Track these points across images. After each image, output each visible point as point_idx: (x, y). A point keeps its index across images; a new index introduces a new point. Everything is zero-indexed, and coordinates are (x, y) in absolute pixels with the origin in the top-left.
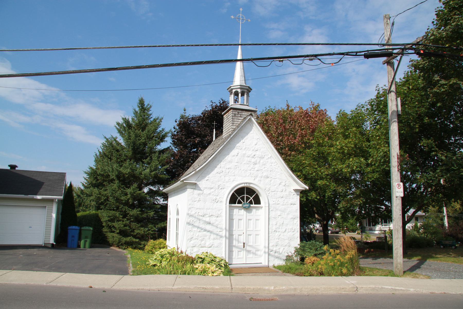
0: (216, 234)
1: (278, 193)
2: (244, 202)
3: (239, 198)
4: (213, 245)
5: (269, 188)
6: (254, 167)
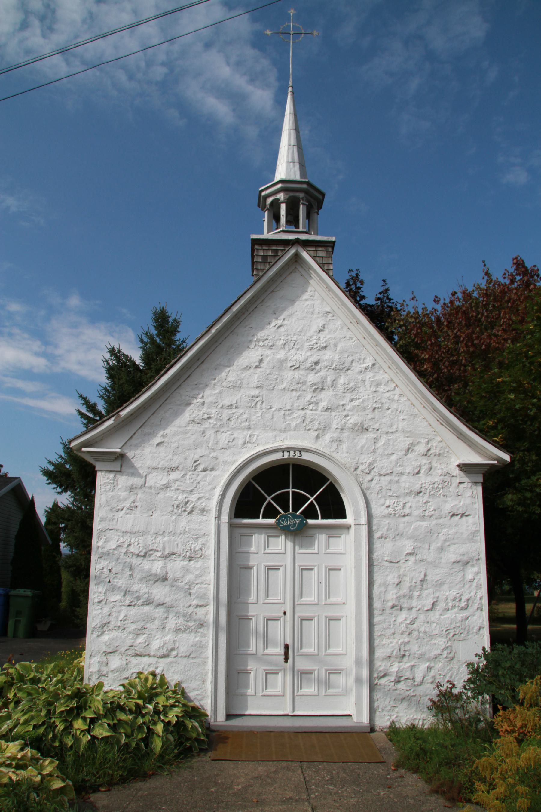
0: (184, 616)
1: (404, 478)
2: (286, 509)
3: (269, 499)
4: (173, 649)
5: (370, 464)
6: (314, 400)
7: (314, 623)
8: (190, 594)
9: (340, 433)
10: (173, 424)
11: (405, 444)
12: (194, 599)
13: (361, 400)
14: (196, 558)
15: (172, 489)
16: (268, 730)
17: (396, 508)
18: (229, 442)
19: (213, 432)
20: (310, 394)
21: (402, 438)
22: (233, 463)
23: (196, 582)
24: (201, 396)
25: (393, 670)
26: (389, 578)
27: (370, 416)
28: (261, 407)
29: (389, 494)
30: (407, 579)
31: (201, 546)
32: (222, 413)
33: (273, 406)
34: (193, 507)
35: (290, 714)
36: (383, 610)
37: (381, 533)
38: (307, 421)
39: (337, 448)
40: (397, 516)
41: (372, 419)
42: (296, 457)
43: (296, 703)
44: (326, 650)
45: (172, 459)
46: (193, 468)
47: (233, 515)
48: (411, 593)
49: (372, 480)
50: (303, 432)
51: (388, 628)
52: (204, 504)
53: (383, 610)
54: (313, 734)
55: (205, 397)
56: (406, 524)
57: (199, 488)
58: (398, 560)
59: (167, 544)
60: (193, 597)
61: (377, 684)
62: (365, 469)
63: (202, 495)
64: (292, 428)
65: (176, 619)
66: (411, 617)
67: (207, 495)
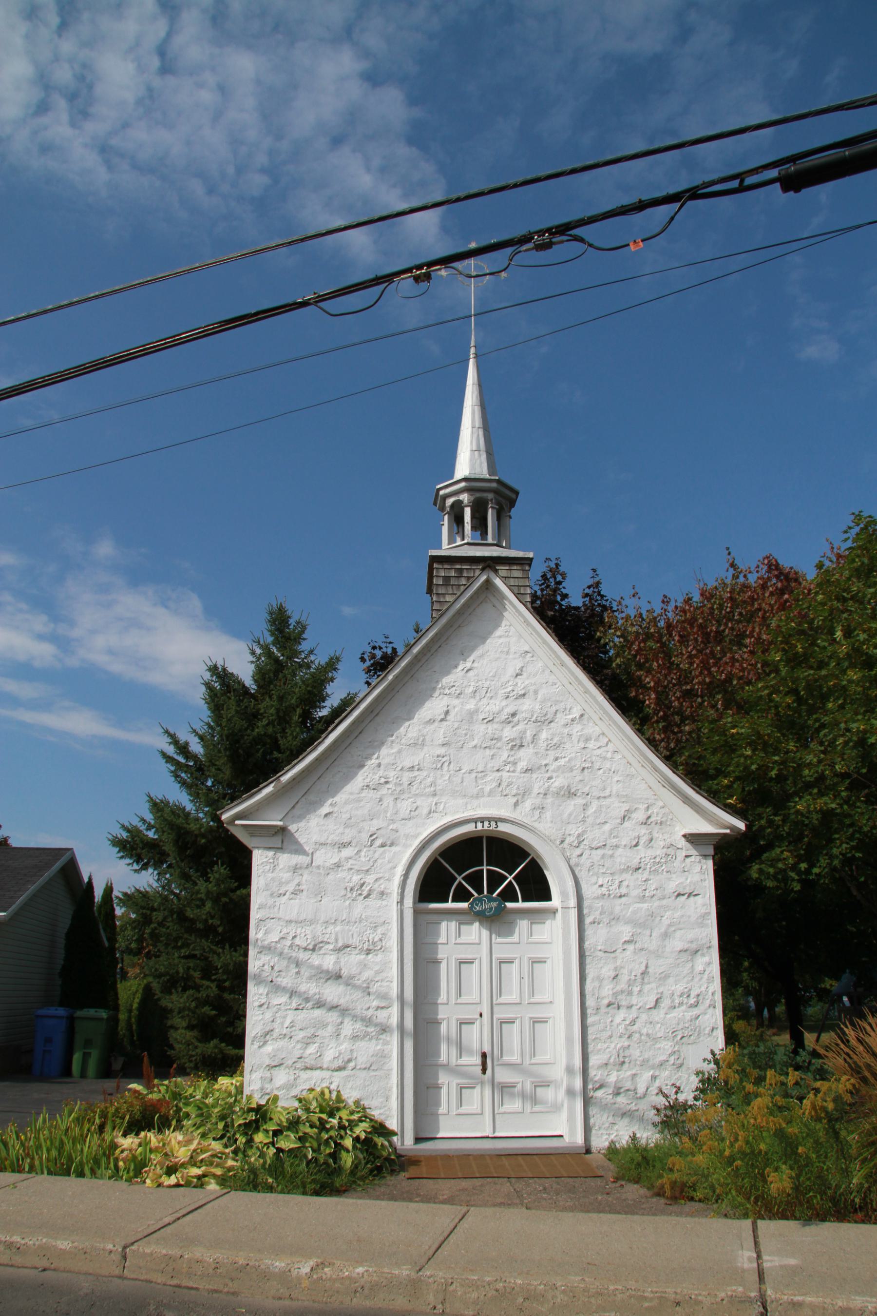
0: (363, 1019)
2: (480, 891)
3: (459, 879)
4: (349, 1061)
5: (579, 836)
6: (511, 759)
7: (516, 1027)
8: (369, 994)
10: (344, 789)
17: (611, 888)
21: (617, 804)
22: (416, 836)
24: (376, 756)
26: (604, 971)
27: (578, 778)
30: (625, 971)
34: (370, 890)
38: (504, 784)
41: (581, 781)
49: (581, 855)
51: (603, 1030)
52: (382, 887)
59: (340, 936)
60: (372, 997)
61: (592, 1097)
63: (381, 875)
64: (486, 794)
67: (387, 875)
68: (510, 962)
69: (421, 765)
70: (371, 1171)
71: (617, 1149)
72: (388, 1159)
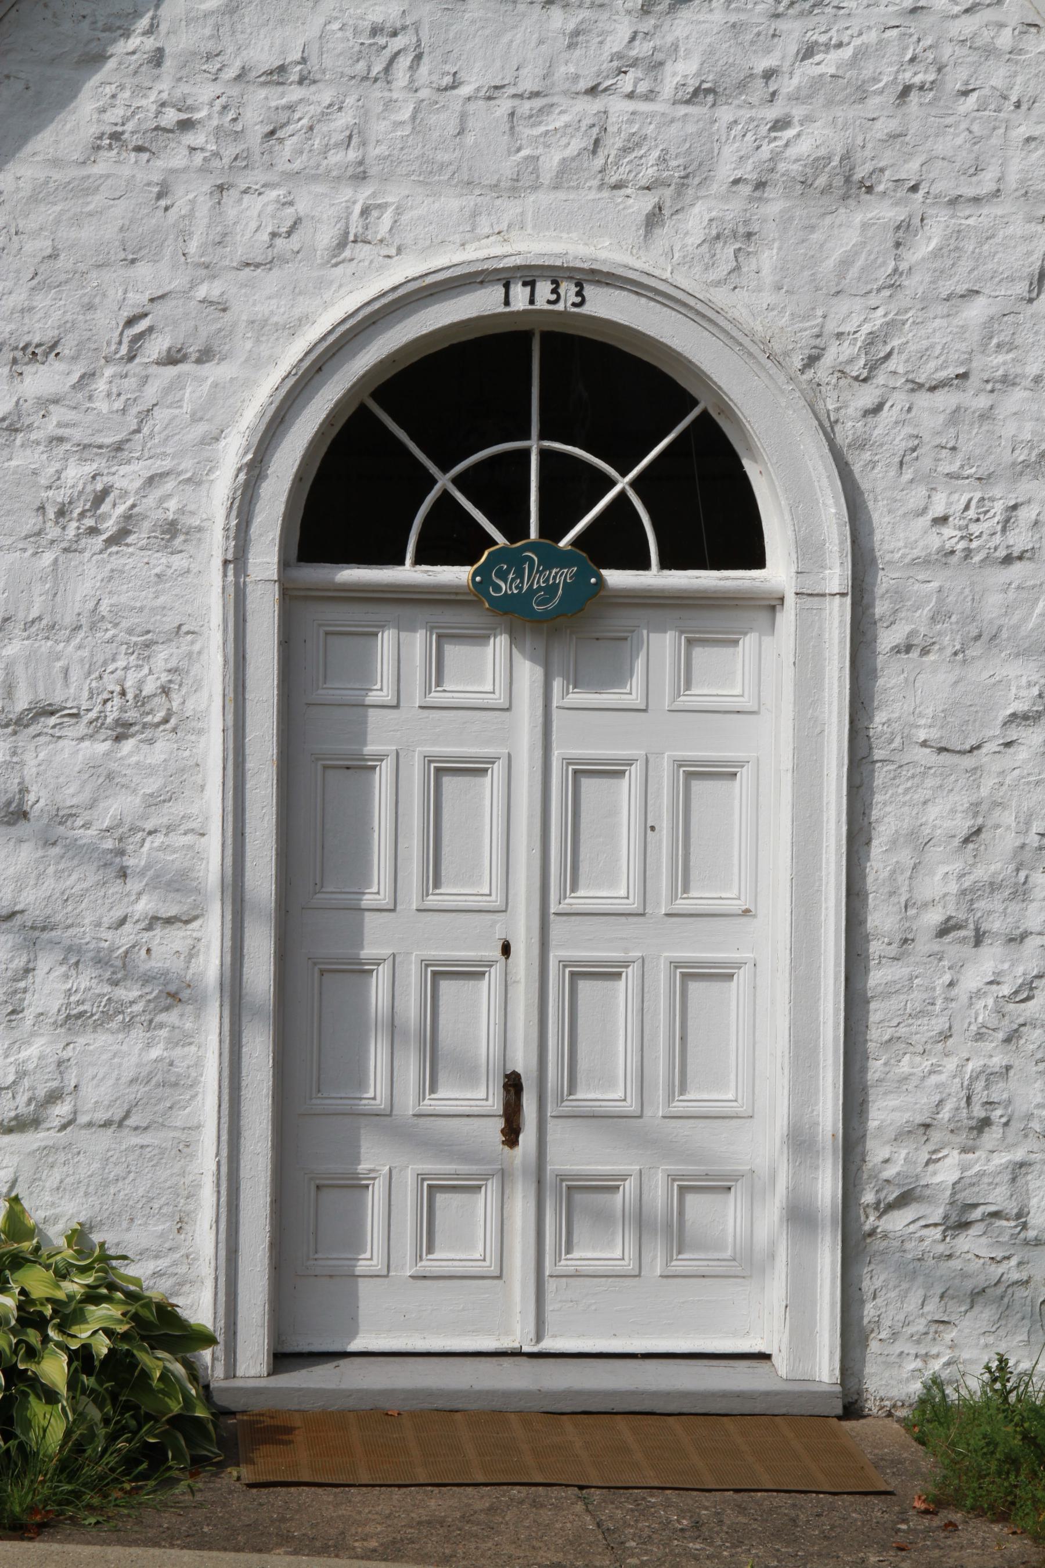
0: (101, 961)
1: (1016, 398)
2: (516, 529)
3: (444, 481)
4: (54, 1097)
5: (872, 339)
6: (642, 49)
7: (623, 991)
8: (123, 874)
9: (751, 199)
10: (29, 148)
11: (1029, 253)
12: (139, 894)
13: (847, 53)
14: (145, 726)
15: (33, 436)
16: (440, 1404)
17: (975, 529)
18: (274, 235)
19: (206, 188)
20: (626, 20)
21: (1018, 227)
22: (293, 329)
23: (149, 826)
24: (144, 22)
25: (937, 1179)
26: (933, 812)
27: (884, 127)
28: (412, 81)
29: (945, 468)
30: (1008, 818)
31: (164, 677)
32: (241, 105)
33: (462, 75)
34: (127, 517)
35: (526, 1349)
36: (905, 941)
37: (908, 629)
38: (613, 144)
39: (737, 268)
40: (977, 559)
41: (894, 137)
42: (560, 307)
43: (549, 1307)
44: (670, 1098)
45: (31, 309)
46: (124, 350)
47: (294, 552)
48: (1022, 875)
49: (877, 409)
50: (593, 195)
51: (921, 1013)
52: (172, 504)
53: (905, 941)
54: (619, 1417)
55: (163, 28)
56: (1011, 594)
57: (152, 436)
58: (972, 741)
59: (20, 671)
60: (134, 885)
61: (872, 1233)
62: (851, 361)
63: (166, 464)
64: (546, 178)
65: (66, 977)
66: (1020, 970)
67: (187, 464)
68: (613, 772)
69: (314, 62)
70: (129, 1462)
71: (948, 1408)
72: (183, 1422)
